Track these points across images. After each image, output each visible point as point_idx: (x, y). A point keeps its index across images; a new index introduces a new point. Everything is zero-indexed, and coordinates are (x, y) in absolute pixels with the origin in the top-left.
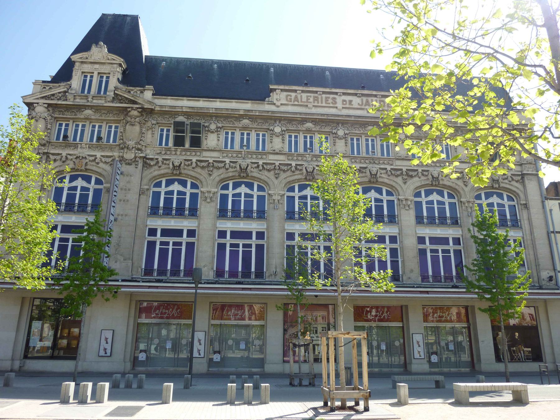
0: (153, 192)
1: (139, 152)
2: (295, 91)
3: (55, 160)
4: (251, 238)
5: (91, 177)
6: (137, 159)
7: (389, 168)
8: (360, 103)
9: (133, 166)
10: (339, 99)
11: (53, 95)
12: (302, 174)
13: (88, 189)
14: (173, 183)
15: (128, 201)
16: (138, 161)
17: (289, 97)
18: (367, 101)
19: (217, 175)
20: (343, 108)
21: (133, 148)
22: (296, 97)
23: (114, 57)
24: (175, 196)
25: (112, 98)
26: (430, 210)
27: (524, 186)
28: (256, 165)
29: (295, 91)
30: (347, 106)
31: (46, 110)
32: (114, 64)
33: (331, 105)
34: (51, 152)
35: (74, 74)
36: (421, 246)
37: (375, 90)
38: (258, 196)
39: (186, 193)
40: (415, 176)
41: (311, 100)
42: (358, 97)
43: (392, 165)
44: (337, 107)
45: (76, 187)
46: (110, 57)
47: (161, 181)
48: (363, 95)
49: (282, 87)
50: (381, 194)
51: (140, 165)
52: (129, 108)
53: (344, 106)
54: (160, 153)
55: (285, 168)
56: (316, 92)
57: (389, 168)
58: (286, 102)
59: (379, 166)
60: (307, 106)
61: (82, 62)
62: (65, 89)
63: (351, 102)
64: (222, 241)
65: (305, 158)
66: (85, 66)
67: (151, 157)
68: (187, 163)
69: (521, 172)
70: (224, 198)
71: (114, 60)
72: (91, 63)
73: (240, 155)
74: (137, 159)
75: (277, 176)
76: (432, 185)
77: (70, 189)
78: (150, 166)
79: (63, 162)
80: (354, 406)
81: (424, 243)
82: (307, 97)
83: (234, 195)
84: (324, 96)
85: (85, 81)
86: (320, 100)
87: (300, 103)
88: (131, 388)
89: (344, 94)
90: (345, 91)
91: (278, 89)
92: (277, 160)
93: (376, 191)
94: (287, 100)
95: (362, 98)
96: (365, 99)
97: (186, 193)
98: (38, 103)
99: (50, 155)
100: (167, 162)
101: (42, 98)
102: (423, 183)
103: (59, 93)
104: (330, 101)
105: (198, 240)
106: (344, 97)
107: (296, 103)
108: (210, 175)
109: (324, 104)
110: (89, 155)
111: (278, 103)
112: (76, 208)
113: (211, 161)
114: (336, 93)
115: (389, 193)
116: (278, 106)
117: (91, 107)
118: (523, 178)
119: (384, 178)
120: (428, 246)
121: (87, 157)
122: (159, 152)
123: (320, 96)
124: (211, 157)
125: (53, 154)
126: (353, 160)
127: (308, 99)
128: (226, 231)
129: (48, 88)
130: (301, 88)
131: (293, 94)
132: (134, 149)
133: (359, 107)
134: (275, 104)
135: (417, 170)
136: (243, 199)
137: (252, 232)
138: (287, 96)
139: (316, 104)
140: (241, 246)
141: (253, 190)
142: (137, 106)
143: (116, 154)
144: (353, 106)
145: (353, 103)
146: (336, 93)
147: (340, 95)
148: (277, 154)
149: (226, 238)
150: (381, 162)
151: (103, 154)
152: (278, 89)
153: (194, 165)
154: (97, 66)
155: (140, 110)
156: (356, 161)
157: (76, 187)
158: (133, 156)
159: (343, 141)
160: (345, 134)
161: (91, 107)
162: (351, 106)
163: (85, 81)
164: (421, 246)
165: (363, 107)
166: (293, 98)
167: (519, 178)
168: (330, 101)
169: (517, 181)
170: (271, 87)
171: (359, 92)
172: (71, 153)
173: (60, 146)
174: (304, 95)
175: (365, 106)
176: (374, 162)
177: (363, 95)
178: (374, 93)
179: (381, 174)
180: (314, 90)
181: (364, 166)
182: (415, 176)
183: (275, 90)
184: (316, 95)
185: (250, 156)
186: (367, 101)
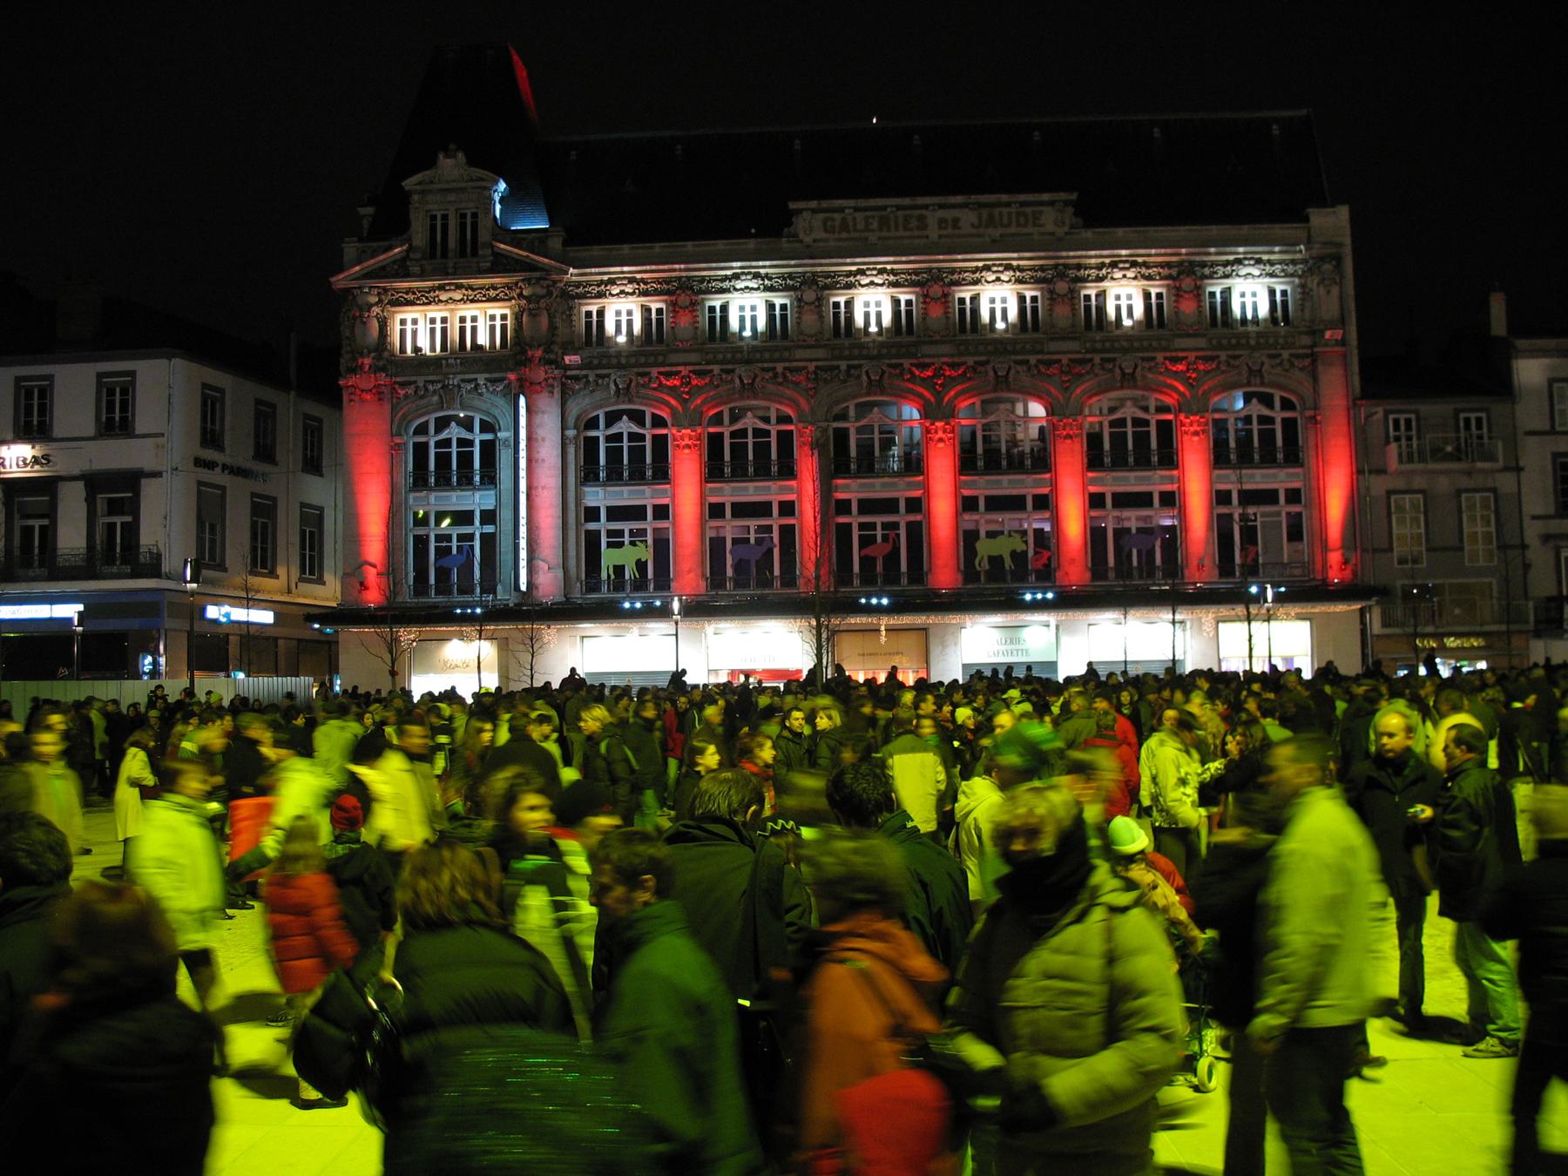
4: (472, 523)
13: (471, 443)
18: (991, 217)
22: (844, 219)
24: (454, 449)
27: (1315, 379)
29: (841, 210)
33: (916, 233)
35: (412, 217)
36: (1223, 510)
37: (1050, 190)
38: (1284, 420)
48: (981, 205)
50: (1270, 405)
51: (557, 391)
55: (827, 376)
56: (884, 208)
58: (824, 235)
61: (423, 192)
63: (956, 221)
64: (592, 526)
68: (1146, 365)
69: (1311, 347)
70: (421, 451)
72: (442, 190)
77: (438, 444)
80: (1139, 802)
82: (866, 218)
83: (609, 439)
84: (900, 213)
85: (433, 228)
86: (892, 224)
89: (941, 206)
92: (811, 360)
93: (630, 419)
94: (826, 230)
96: (985, 213)
100: (1237, 363)
104: (914, 223)
105: (674, 524)
106: (941, 213)
114: (926, 207)
115: (1287, 405)
118: (1314, 362)
120: (854, 519)
124: (685, 364)
127: (867, 224)
130: (852, 203)
131: (837, 216)
133: (974, 231)
135: (1091, 360)
136: (750, 440)
138: (825, 221)
139: (884, 234)
140: (879, 527)
146: (926, 207)
149: (645, 519)
154: (451, 197)
163: (433, 228)
164: (1223, 510)
166: (837, 223)
167: (1307, 362)
168: (914, 223)
169: (1301, 369)
171: (973, 198)
174: (860, 216)
178: (1004, 198)
183: (800, 211)
186: (991, 217)
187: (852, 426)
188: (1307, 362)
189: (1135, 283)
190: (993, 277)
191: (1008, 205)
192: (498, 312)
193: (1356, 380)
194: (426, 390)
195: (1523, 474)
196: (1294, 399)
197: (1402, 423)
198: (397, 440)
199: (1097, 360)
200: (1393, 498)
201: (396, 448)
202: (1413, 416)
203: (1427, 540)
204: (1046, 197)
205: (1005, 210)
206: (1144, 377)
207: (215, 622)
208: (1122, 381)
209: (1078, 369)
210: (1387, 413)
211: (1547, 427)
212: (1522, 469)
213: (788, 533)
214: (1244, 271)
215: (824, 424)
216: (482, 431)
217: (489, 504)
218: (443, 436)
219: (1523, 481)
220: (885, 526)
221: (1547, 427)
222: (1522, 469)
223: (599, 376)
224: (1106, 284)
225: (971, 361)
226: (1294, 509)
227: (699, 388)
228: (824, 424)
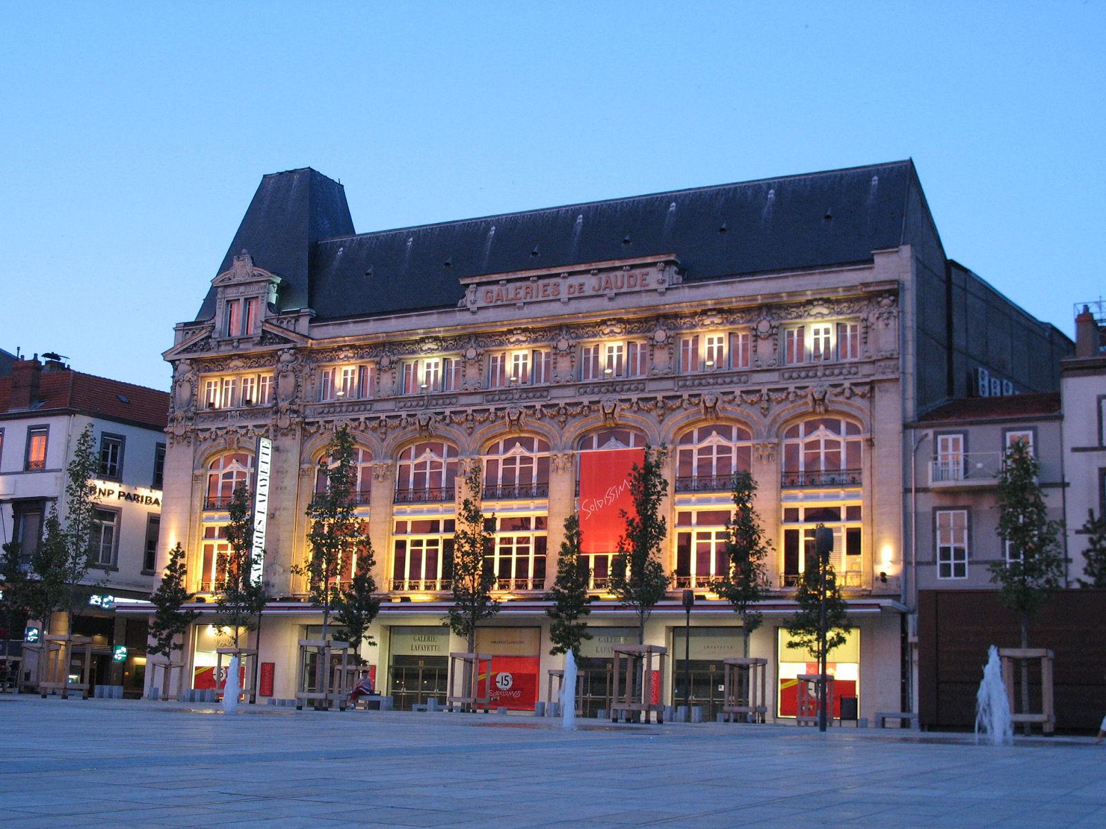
0: (786, 445)
1: (295, 416)
2: (496, 282)
3: (205, 439)
5: (532, 439)
6: (293, 427)
7: (634, 397)
8: (597, 287)
9: (290, 437)
10: (564, 284)
11: (195, 345)
12: (806, 403)
13: (729, 450)
14: (817, 428)
15: (285, 488)
16: (294, 430)
17: (489, 294)
19: (574, 429)
20: (570, 299)
21: (287, 410)
23: (261, 271)
24: (714, 456)
25: (259, 338)
26: (813, 460)
28: (441, 417)
30: (576, 295)
31: (293, 358)
32: (263, 281)
34: (200, 427)
39: (839, 443)
40: (678, 408)
41: (522, 293)
42: (593, 274)
43: (643, 390)
44: (559, 300)
45: (818, 442)
46: (255, 272)
47: (691, 433)
48: (600, 270)
49: (477, 280)
51: (298, 434)
52: (280, 350)
53: (571, 296)
54: (322, 412)
57: (634, 397)
59: (619, 397)
60: (515, 304)
62: (207, 334)
65: (511, 396)
66: (229, 291)
67: (311, 420)
68: (727, 398)
71: (262, 275)
72: (236, 285)
73: (421, 403)
74: (293, 427)
75: (765, 412)
76: (814, 413)
78: (311, 435)
79: (214, 440)
81: (849, 518)
83: (701, 451)
84: (541, 282)
87: (505, 303)
88: (866, 727)
89: (571, 274)
90: (511, 276)
91: (472, 284)
95: (600, 276)
96: (603, 276)
97: (731, 448)
98: (179, 360)
99: (199, 432)
101: (184, 351)
102: (691, 419)
103: (202, 340)
107: (499, 303)
108: (383, 440)
109: (540, 299)
110: (240, 427)
111: (473, 308)
112: (517, 491)
113: (562, 403)
114: (558, 275)
116: (474, 313)
117: (240, 356)
118: (872, 390)
119: (839, 403)
121: (239, 430)
122: (321, 410)
123: (534, 285)
124: (383, 411)
125: (202, 430)
126: (582, 390)
128: (406, 522)
129: (190, 332)
130: (504, 276)
131: (495, 288)
132: (288, 412)
133: (594, 293)
134: (469, 309)
135: (681, 396)
137: (406, 522)
140: (713, 536)
141: (839, 433)
142: (288, 346)
143: (269, 422)
144: (587, 294)
145: (585, 288)
146: (558, 275)
147: (564, 278)
148: (471, 394)
150: (626, 387)
151: (255, 424)
152: (472, 284)
153: (847, 393)
154: (242, 289)
155: (292, 351)
156: (586, 392)
157: (818, 442)
158: (288, 422)
159: (568, 359)
160: (570, 347)
161: (240, 356)
162: (582, 295)
165: (600, 292)
166: (495, 294)
170: (462, 282)
171: (594, 266)
172: (220, 426)
173: (209, 417)
174: (511, 286)
175: (604, 290)
176: (615, 390)
177: (600, 270)
178: (617, 264)
179: (623, 410)
180: (524, 276)
181: (595, 398)
182: (678, 408)
183: (467, 286)
184: (528, 283)
185: (434, 402)
187: (801, 441)
188: (867, 388)
189: (721, 328)
190: (607, 331)
191: (620, 268)
192: (615, 345)
193: (910, 405)
194: (217, 435)
195: (1067, 489)
196: (860, 427)
197: (950, 444)
198: (197, 472)
199: (686, 396)
200: (938, 513)
201: (195, 478)
202: (961, 437)
203: (970, 555)
204: (649, 260)
205: (619, 273)
206: (724, 409)
207: (98, 607)
208: (706, 413)
209: (670, 403)
210: (936, 434)
211: (1095, 444)
212: (1068, 485)
213: (541, 544)
214: (814, 311)
215: (570, 452)
216: (449, 455)
217: (542, 513)
218: (705, 444)
219: (1067, 495)
220: (520, 541)
221: (1095, 444)
222: (1068, 485)
223: (327, 422)
224: (698, 330)
225: (585, 400)
226: (854, 525)
227: (481, 423)
228: (570, 452)
